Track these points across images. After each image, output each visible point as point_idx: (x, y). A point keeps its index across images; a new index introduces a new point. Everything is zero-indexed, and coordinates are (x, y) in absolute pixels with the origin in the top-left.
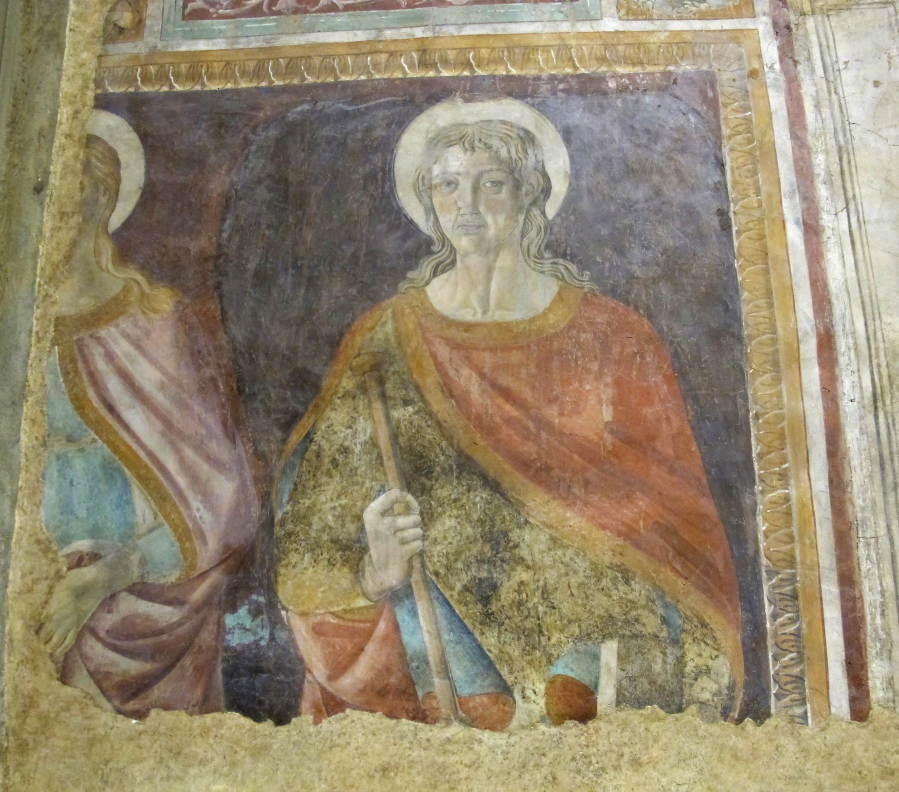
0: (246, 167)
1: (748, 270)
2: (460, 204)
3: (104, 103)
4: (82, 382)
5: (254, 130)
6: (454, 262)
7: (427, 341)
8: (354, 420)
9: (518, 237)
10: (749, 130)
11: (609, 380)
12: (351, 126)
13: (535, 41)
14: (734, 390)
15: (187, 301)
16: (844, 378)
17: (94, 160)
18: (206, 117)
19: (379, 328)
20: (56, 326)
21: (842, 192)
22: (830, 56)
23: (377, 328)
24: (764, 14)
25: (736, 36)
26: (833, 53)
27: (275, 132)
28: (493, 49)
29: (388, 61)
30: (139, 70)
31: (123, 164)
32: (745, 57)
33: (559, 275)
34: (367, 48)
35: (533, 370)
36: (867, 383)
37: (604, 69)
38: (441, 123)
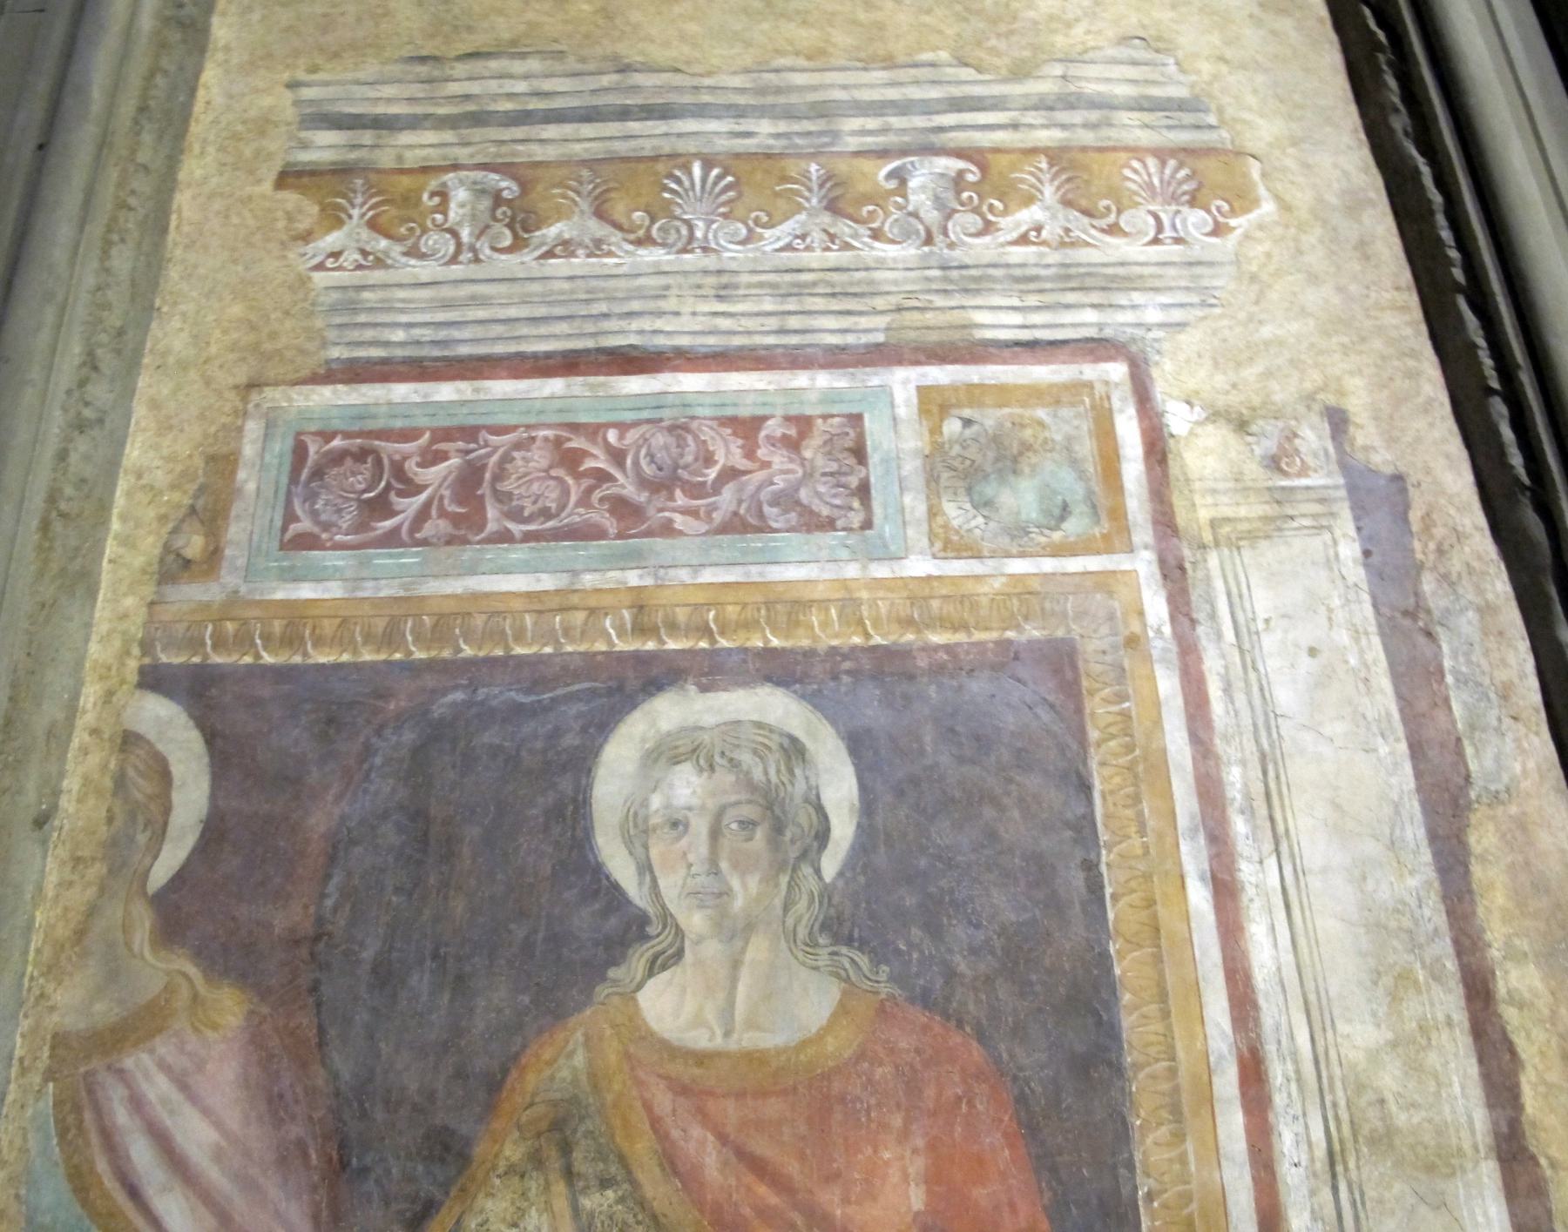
0: (365, 791)
1: (1129, 957)
2: (691, 858)
3: (154, 680)
4: (88, 1144)
5: (379, 732)
6: (679, 954)
7: (640, 1083)
8: (522, 1212)
9: (779, 911)
10: (1126, 732)
11: (920, 1142)
12: (528, 728)
13: (807, 594)
14: (1114, 1154)
15: (265, 1010)
16: (1282, 1128)
17: (131, 772)
18: (308, 707)
19: (564, 1060)
20: (53, 1048)
21: (1268, 824)
22: (1244, 610)
23: (562, 1061)
24: (1146, 547)
25: (1104, 582)
26: (1247, 605)
27: (413, 736)
28: (745, 605)
29: (586, 623)
30: (210, 628)
31: (177, 782)
32: (1119, 614)
33: (843, 973)
34: (554, 603)
35: (803, 1129)
36: (1318, 1134)
37: (910, 637)
38: (665, 726)
